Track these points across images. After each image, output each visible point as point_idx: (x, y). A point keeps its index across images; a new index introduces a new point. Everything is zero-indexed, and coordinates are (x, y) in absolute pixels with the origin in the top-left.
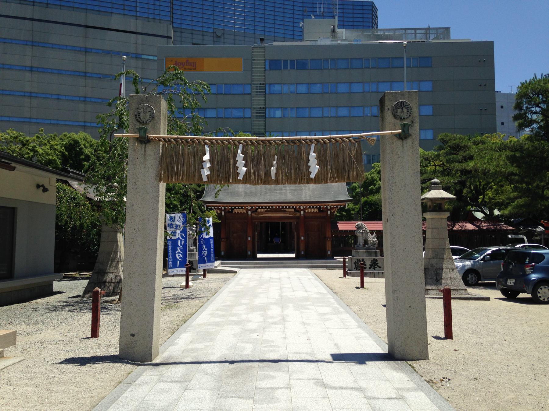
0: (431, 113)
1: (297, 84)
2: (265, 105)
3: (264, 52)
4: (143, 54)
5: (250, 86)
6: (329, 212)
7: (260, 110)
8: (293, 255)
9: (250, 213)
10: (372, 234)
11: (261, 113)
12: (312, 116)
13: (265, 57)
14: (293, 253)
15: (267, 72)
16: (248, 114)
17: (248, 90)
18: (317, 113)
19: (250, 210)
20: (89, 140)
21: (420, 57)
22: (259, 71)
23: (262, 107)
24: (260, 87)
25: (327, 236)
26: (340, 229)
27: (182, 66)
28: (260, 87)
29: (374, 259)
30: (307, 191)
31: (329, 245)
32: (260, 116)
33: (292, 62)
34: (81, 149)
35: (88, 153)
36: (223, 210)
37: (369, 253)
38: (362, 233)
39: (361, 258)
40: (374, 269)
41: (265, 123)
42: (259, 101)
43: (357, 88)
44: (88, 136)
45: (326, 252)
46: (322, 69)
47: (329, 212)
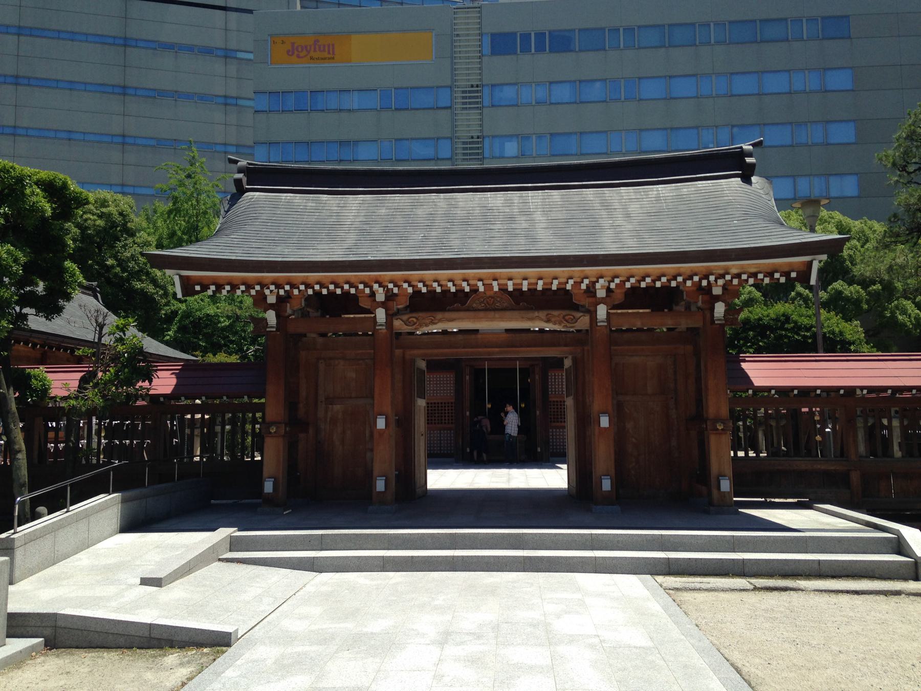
2: (481, 131)
3: (480, 18)
5: (448, 90)
7: (470, 143)
13: (480, 29)
15: (485, 59)
17: (444, 101)
21: (823, 18)
22: (468, 58)
23: (475, 134)
24: (470, 92)
27: (304, 53)
28: (470, 92)
30: (620, 221)
32: (470, 154)
33: (540, 36)
36: (272, 306)
45: (703, 476)
46: (604, 50)
47: (720, 309)
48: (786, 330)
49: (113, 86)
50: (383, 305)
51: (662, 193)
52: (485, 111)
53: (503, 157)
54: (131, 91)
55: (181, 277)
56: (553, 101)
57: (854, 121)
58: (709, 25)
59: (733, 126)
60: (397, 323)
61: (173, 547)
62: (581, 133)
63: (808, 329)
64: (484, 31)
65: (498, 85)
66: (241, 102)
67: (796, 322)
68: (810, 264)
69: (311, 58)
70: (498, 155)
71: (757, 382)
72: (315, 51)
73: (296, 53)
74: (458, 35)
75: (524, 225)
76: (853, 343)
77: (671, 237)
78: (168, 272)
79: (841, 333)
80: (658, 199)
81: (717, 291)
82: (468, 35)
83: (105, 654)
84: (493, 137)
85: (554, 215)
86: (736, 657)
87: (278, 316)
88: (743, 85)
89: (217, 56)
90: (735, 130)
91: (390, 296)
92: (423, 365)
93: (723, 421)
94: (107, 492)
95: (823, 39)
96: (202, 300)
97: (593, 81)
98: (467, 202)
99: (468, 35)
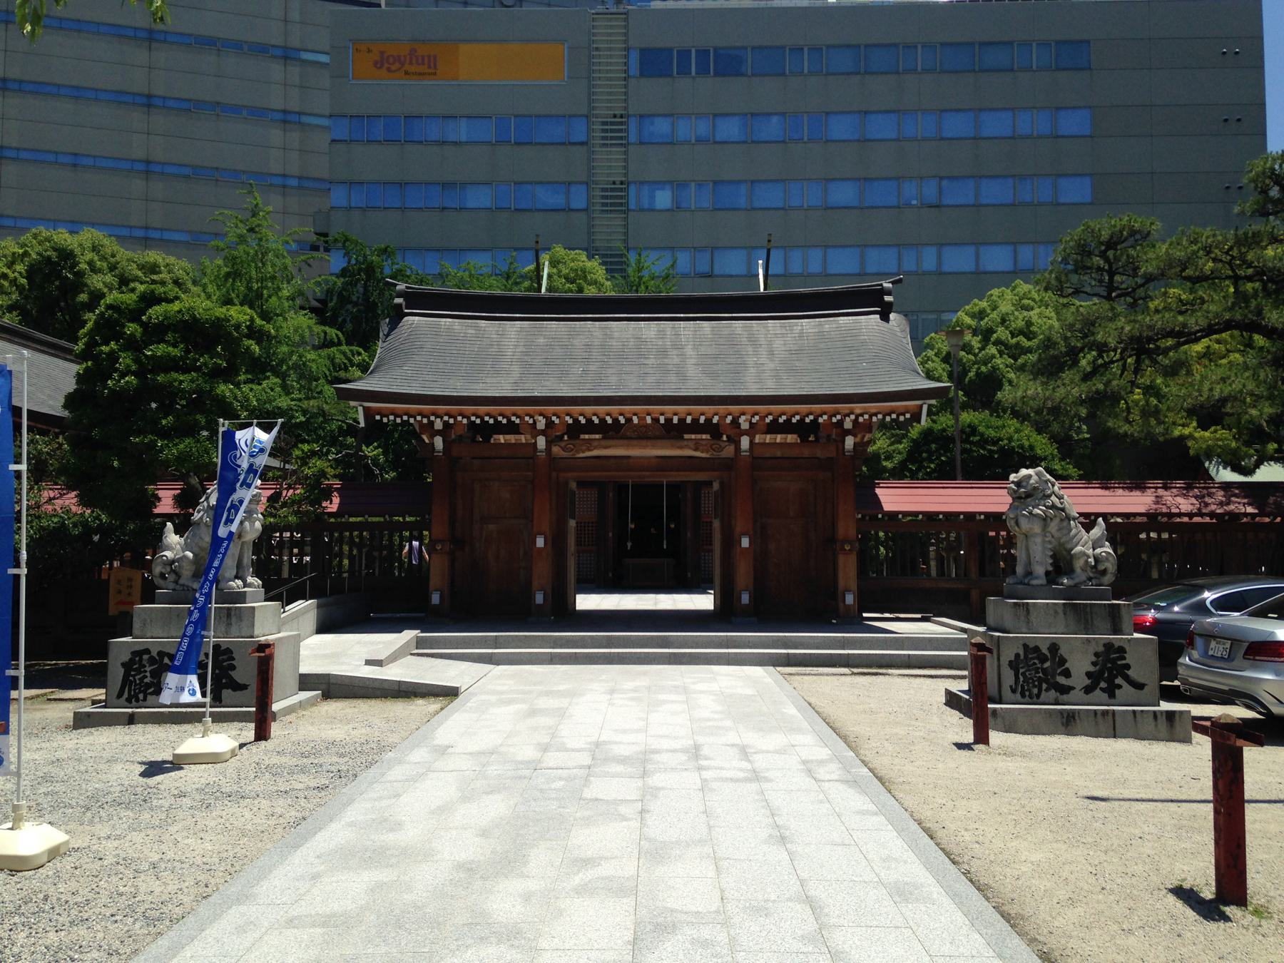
0: (1088, 199)
1: (715, 115)
2: (626, 175)
4: (305, 50)
5: (584, 119)
6: (850, 442)
7: (612, 190)
8: (704, 602)
9: (541, 442)
10: (1088, 527)
11: (616, 198)
12: (757, 204)
13: (626, 41)
14: (703, 591)
15: (632, 82)
16: (579, 201)
18: (771, 196)
19: (543, 433)
20: (109, 251)
21: (1057, 42)
22: (610, 79)
23: (618, 179)
24: (612, 123)
25: (841, 532)
26: (887, 507)
27: (397, 65)
28: (612, 123)
29: (1109, 646)
31: (847, 570)
33: (704, 54)
34: (80, 274)
35: (100, 285)
36: (439, 433)
37: (1082, 618)
38: (1045, 520)
39: (1042, 637)
40: (1111, 692)
41: (626, 226)
42: (609, 164)
43: (883, 127)
44: (106, 242)
45: (834, 594)
46: (783, 74)
47: (850, 442)
48: (971, 443)
49: (134, 94)
50: (543, 433)
51: (807, 326)
52: (631, 148)
53: (653, 210)
54: (159, 102)
55: (364, 408)
56: (718, 139)
57: (1091, 175)
58: (916, 47)
59: (941, 178)
60: (556, 449)
61: (372, 643)
62: (752, 182)
63: (995, 442)
64: (631, 43)
65: (650, 116)
66: (304, 119)
67: (982, 435)
68: (921, 407)
69: (406, 73)
70: (646, 206)
71: (887, 507)
72: (411, 63)
73: (386, 65)
74: (597, 49)
75: (676, 360)
76: (1045, 459)
77: (806, 379)
78: (352, 403)
79: (1032, 448)
80: (801, 334)
81: (848, 424)
82: (610, 49)
83: (373, 702)
84: (642, 183)
85: (703, 350)
86: (813, 700)
87: (444, 441)
88: (957, 125)
89: (274, 57)
90: (945, 183)
91: (550, 424)
92: (573, 485)
93: (850, 543)
94: (304, 598)
95: (1058, 69)
96: (272, 390)
97: (769, 115)
98: (622, 331)
99: (610, 49)
